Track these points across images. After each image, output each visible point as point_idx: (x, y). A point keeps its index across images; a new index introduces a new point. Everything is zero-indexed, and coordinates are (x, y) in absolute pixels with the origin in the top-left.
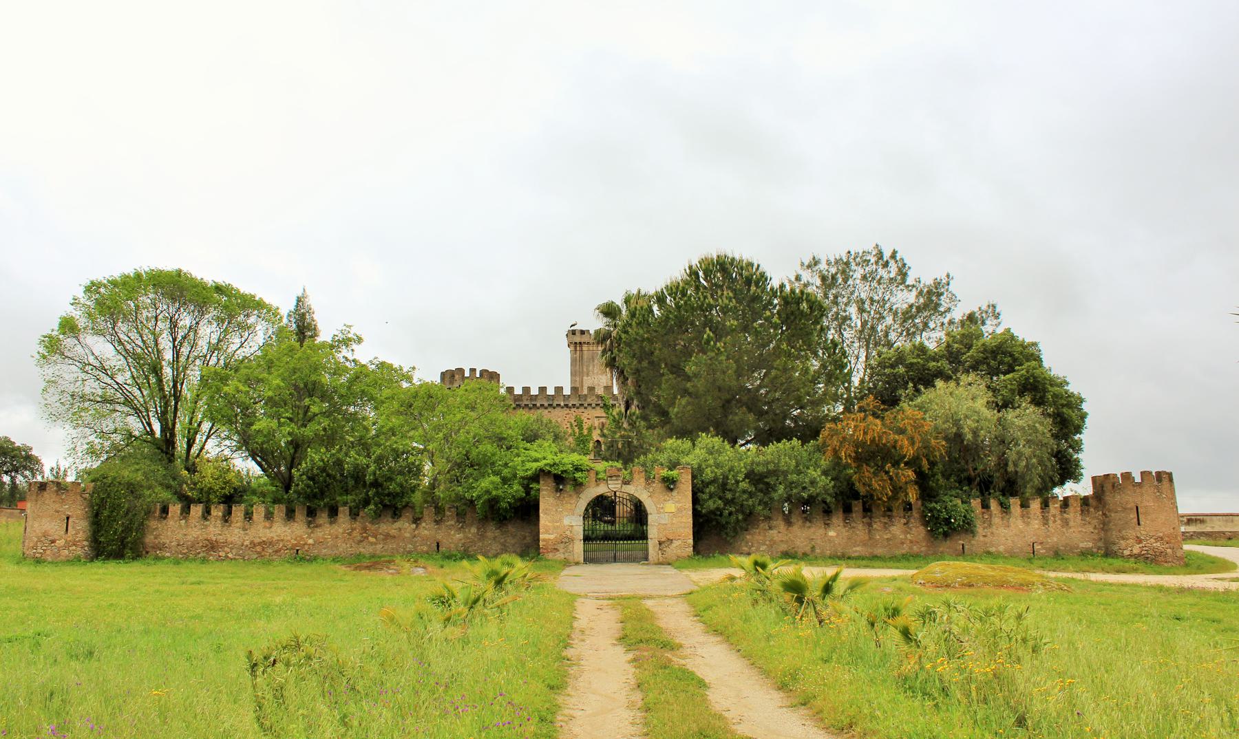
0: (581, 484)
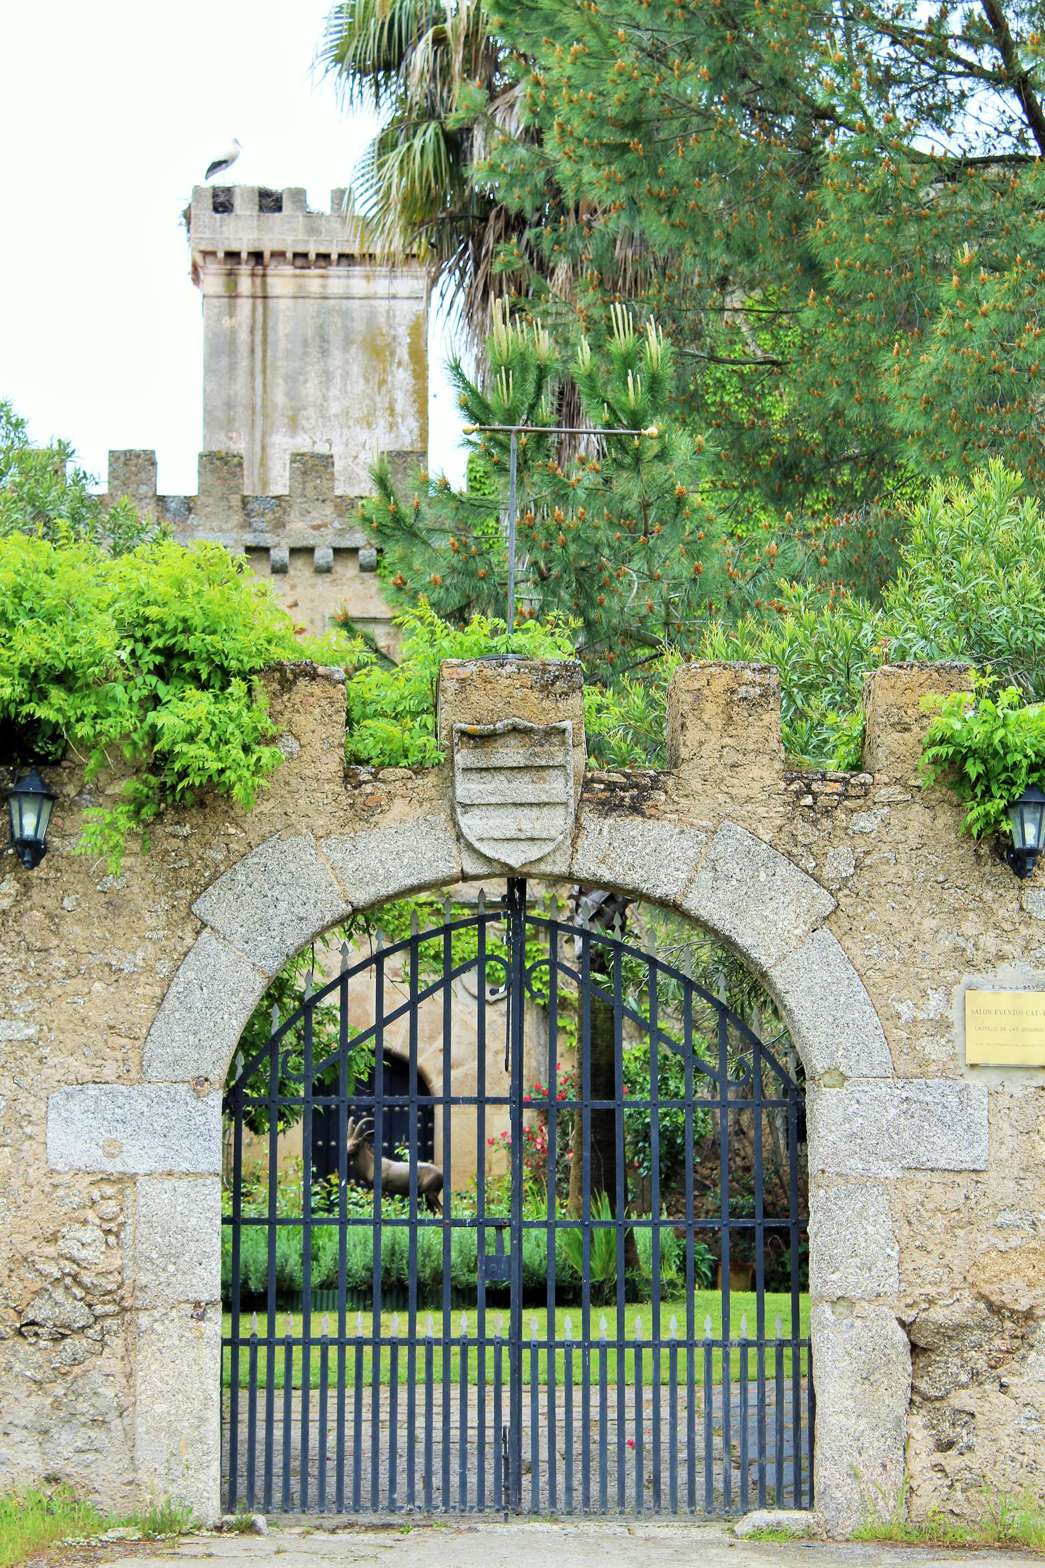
0: (208, 798)
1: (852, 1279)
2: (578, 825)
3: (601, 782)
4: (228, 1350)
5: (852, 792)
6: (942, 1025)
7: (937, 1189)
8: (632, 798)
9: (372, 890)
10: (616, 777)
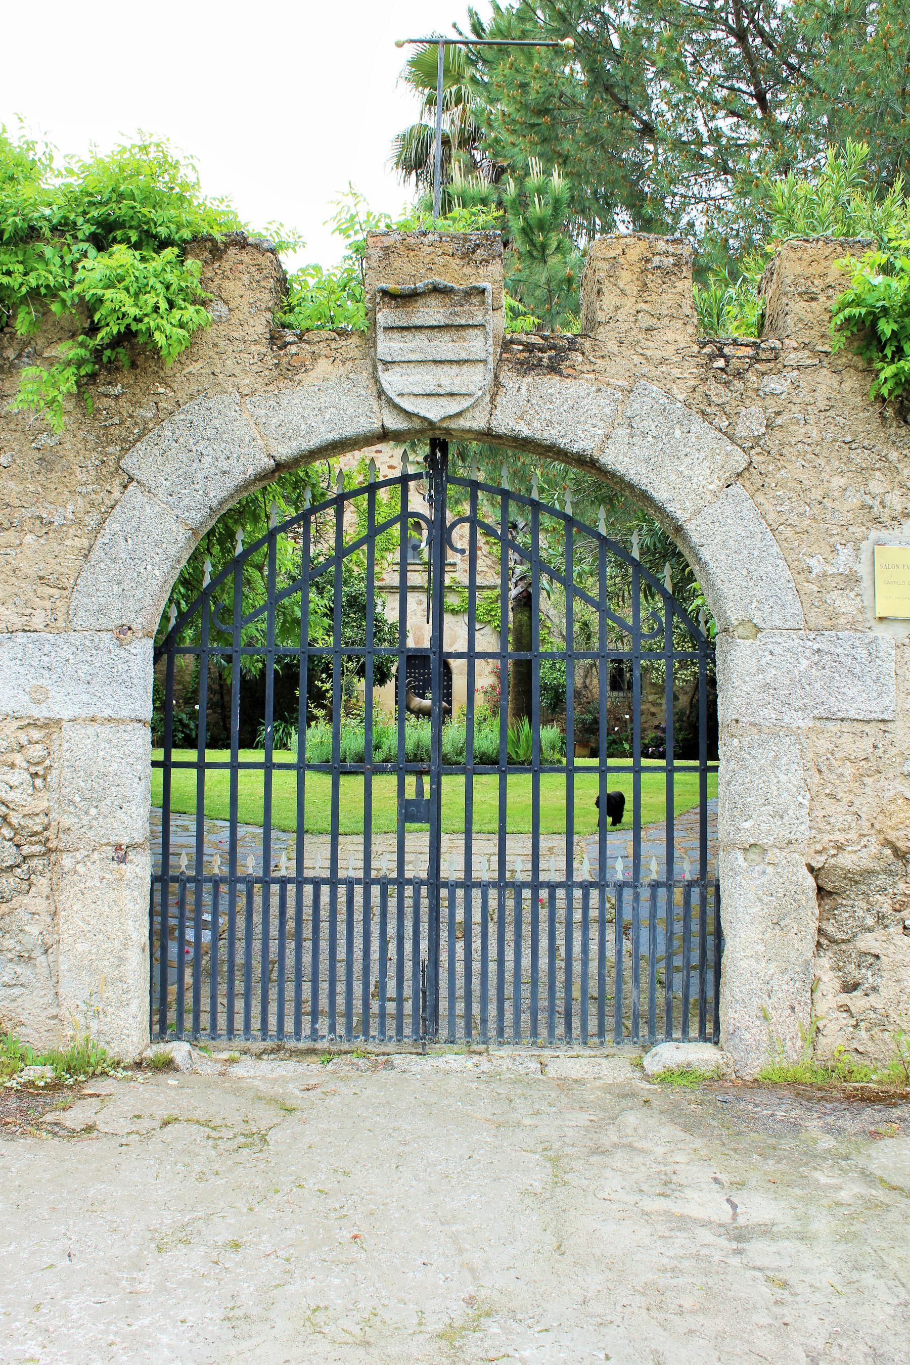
1: (764, 827)
2: (497, 383)
3: (520, 343)
4: (158, 886)
5: (763, 356)
6: (851, 580)
7: (847, 739)
8: (550, 358)
9: (294, 444)
10: (535, 339)
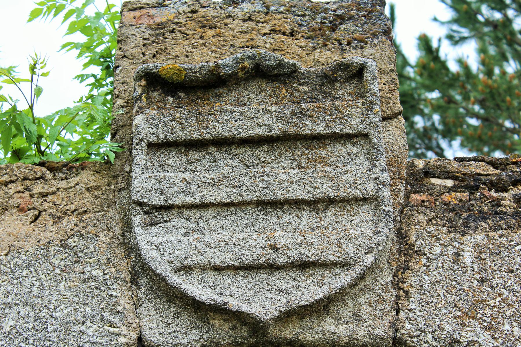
2: (404, 246)
